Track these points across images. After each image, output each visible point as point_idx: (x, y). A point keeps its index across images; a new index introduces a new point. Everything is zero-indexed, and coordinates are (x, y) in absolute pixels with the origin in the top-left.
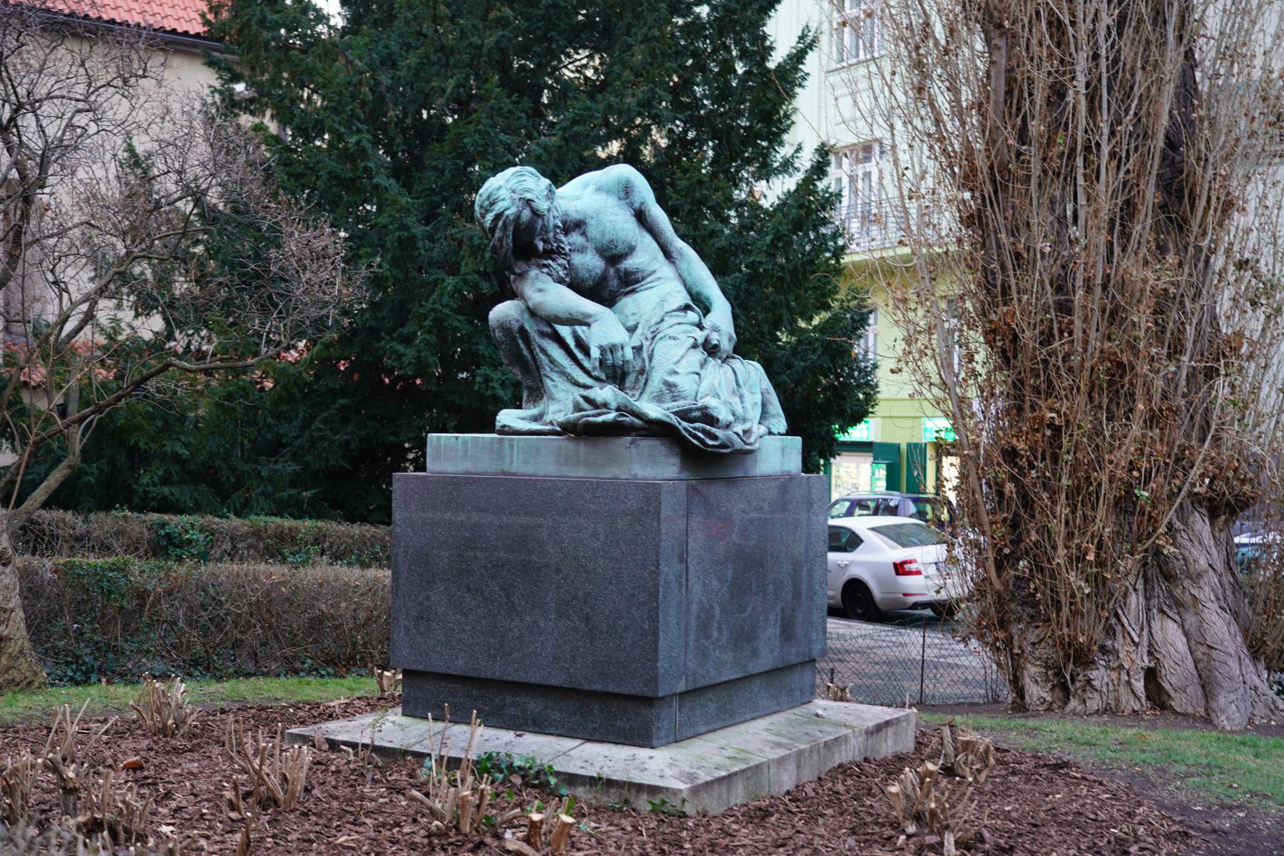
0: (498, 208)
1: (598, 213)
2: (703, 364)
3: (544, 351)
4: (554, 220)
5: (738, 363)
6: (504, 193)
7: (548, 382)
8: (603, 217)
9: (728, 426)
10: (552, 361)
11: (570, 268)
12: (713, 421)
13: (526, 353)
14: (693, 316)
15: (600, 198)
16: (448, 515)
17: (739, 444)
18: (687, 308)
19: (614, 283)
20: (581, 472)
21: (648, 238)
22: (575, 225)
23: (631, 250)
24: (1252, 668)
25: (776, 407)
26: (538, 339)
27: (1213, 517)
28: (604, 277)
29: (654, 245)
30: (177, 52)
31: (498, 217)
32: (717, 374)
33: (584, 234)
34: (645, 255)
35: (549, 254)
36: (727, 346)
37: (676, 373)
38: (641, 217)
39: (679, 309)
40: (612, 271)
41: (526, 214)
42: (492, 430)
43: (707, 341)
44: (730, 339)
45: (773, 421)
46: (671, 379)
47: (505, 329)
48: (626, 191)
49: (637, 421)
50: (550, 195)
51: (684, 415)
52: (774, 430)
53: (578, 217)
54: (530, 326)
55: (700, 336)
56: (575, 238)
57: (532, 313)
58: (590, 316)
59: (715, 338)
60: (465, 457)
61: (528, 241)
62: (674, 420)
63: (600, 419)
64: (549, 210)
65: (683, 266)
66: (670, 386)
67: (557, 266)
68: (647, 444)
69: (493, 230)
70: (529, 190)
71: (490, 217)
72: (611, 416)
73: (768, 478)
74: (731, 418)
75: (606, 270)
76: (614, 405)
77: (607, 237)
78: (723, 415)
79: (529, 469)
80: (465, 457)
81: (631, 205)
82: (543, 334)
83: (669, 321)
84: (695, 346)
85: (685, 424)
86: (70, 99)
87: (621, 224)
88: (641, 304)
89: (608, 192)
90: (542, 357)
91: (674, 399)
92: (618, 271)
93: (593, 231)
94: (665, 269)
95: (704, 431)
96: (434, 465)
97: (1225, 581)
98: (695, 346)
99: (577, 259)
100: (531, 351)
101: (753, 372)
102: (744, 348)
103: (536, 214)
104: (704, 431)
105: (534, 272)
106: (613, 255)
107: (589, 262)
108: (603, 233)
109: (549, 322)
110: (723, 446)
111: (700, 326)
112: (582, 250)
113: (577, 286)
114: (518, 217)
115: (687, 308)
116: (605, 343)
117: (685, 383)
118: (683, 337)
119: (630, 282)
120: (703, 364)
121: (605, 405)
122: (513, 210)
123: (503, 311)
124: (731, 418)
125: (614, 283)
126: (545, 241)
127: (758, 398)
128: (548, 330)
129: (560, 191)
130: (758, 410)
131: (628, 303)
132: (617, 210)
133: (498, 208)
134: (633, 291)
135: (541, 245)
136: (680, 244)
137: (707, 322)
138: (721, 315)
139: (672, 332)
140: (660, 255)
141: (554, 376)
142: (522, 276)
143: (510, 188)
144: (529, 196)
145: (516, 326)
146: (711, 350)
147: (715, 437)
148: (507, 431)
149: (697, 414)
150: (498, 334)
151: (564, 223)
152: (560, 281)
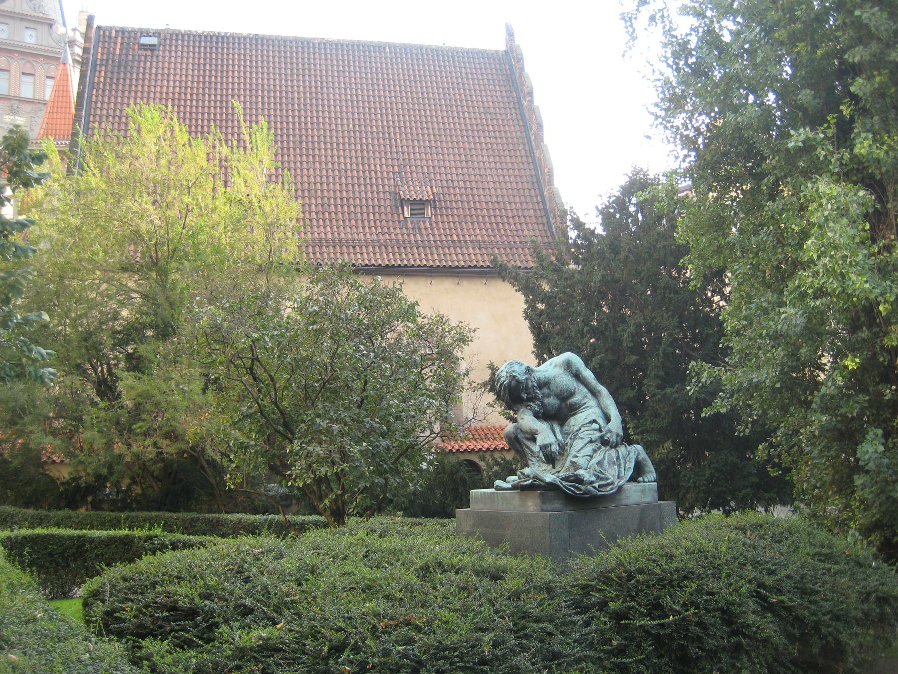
0: (502, 380)
1: (554, 377)
2: (595, 451)
8: (557, 380)
9: (592, 483)
14: (595, 426)
18: (594, 421)
21: (582, 387)
22: (544, 384)
23: (572, 394)
28: (560, 409)
29: (585, 390)
30: (407, 275)
31: (501, 385)
33: (549, 388)
34: (581, 395)
37: (576, 457)
38: (577, 376)
41: (514, 383)
43: (602, 437)
44: (617, 435)
45: (648, 475)
46: (574, 460)
48: (568, 366)
52: (646, 480)
56: (546, 391)
64: (527, 379)
70: (514, 372)
74: (593, 479)
75: (561, 405)
81: (571, 372)
82: (528, 439)
84: (591, 441)
85: (564, 483)
87: (566, 381)
88: (576, 421)
93: (553, 387)
94: (592, 402)
98: (591, 441)
99: (546, 401)
103: (519, 382)
106: (565, 396)
107: (552, 401)
110: (584, 493)
111: (600, 430)
112: (549, 396)
114: (510, 383)
115: (594, 421)
119: (574, 409)
120: (595, 451)
121: (528, 476)
126: (528, 394)
127: (632, 465)
134: (575, 414)
135: (525, 396)
138: (616, 425)
140: (589, 395)
144: (514, 374)
146: (604, 442)
147: (579, 489)
148: (498, 488)
151: (539, 385)
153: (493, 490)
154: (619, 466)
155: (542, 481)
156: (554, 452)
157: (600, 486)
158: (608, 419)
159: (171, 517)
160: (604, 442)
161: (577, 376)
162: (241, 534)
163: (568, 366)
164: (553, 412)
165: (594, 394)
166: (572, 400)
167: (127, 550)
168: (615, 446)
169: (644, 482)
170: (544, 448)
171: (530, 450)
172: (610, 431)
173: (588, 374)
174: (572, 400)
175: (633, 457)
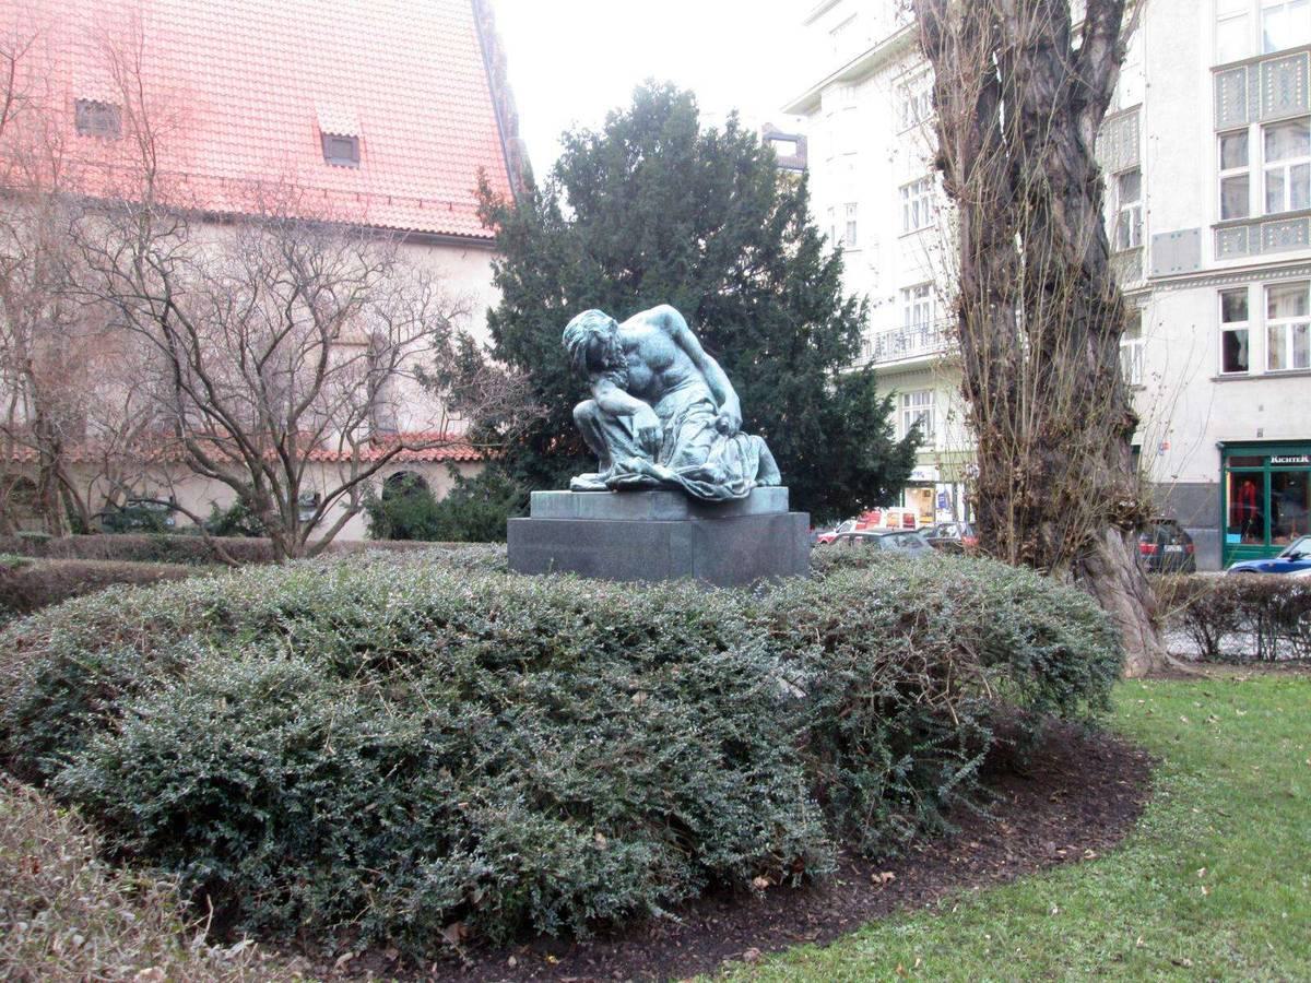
0: (575, 339)
1: (647, 339)
2: (713, 440)
3: (609, 433)
4: (616, 345)
5: (743, 439)
6: (580, 328)
7: (613, 455)
9: (722, 482)
10: (615, 440)
11: (629, 377)
12: (709, 479)
13: (597, 434)
15: (646, 328)
16: (540, 547)
17: (729, 494)
19: (660, 385)
20: (619, 517)
22: (631, 348)
23: (670, 363)
24: (1152, 635)
25: (773, 465)
26: (606, 425)
27: (1125, 529)
28: (652, 383)
29: (687, 358)
31: (575, 345)
32: (723, 445)
33: (638, 353)
34: (681, 365)
35: (613, 367)
36: (733, 425)
37: (690, 446)
38: (678, 340)
39: (700, 402)
40: (658, 377)
41: (594, 341)
42: (568, 488)
43: (718, 423)
44: (737, 421)
46: (688, 450)
47: (583, 418)
48: (666, 323)
49: (656, 481)
50: (612, 328)
51: (689, 475)
53: (634, 342)
54: (599, 417)
55: (712, 419)
56: (633, 356)
57: (601, 408)
58: (633, 409)
59: (725, 421)
60: (551, 508)
61: (598, 360)
62: (681, 479)
63: (630, 480)
65: (708, 372)
66: (687, 455)
67: (619, 376)
68: (667, 497)
69: (572, 353)
70: (595, 326)
71: (571, 344)
72: (637, 478)
73: (758, 517)
74: (724, 476)
76: (640, 470)
77: (654, 354)
78: (718, 474)
79: (591, 515)
80: (551, 508)
81: (670, 332)
82: (610, 423)
83: (692, 410)
84: (708, 427)
85: (689, 481)
86: (227, 336)
87: (661, 344)
88: (676, 401)
89: (655, 324)
90: (608, 437)
91: (689, 464)
92: (662, 377)
93: (644, 351)
94: (695, 375)
95: (702, 486)
96: (537, 514)
97: (1134, 576)
98: (708, 427)
99: (634, 370)
100: (601, 434)
101: (756, 444)
102: (748, 427)
103: (601, 341)
104: (702, 486)
105: (602, 381)
106: (659, 366)
107: (642, 372)
108: (650, 352)
109: (615, 416)
111: (714, 413)
112: (637, 364)
113: (633, 391)
114: (588, 343)
116: (642, 427)
117: (697, 452)
118: (700, 420)
119: (671, 384)
120: (713, 440)
121: (634, 470)
122: (585, 339)
123: (583, 407)
124: (724, 476)
125: (660, 385)
127: (757, 461)
128: (611, 419)
129: (620, 326)
130: (756, 471)
131: (669, 400)
132: (660, 337)
133: (575, 339)
135: (607, 362)
136: (706, 357)
137: (720, 411)
138: (732, 407)
139: (692, 418)
141: (617, 450)
142: (595, 383)
143: (587, 324)
145: (590, 417)
146: (722, 429)
147: (709, 490)
148: (576, 489)
149: (698, 474)
150: (579, 423)
152: (621, 386)
153: (569, 492)
154: (742, 461)
155: (656, 477)
156: (657, 440)
157: (734, 486)
158: (719, 398)
159: (467, 955)
160: (722, 429)
161: (678, 340)
162: (812, 244)
163: (666, 323)
164: (643, 387)
165: (698, 364)
166: (670, 372)
167: (93, 582)
168: (732, 436)
169: (768, 485)
170: (645, 432)
171: (612, 436)
172: (727, 415)
173: (691, 337)
174: (670, 372)
175: (755, 450)
